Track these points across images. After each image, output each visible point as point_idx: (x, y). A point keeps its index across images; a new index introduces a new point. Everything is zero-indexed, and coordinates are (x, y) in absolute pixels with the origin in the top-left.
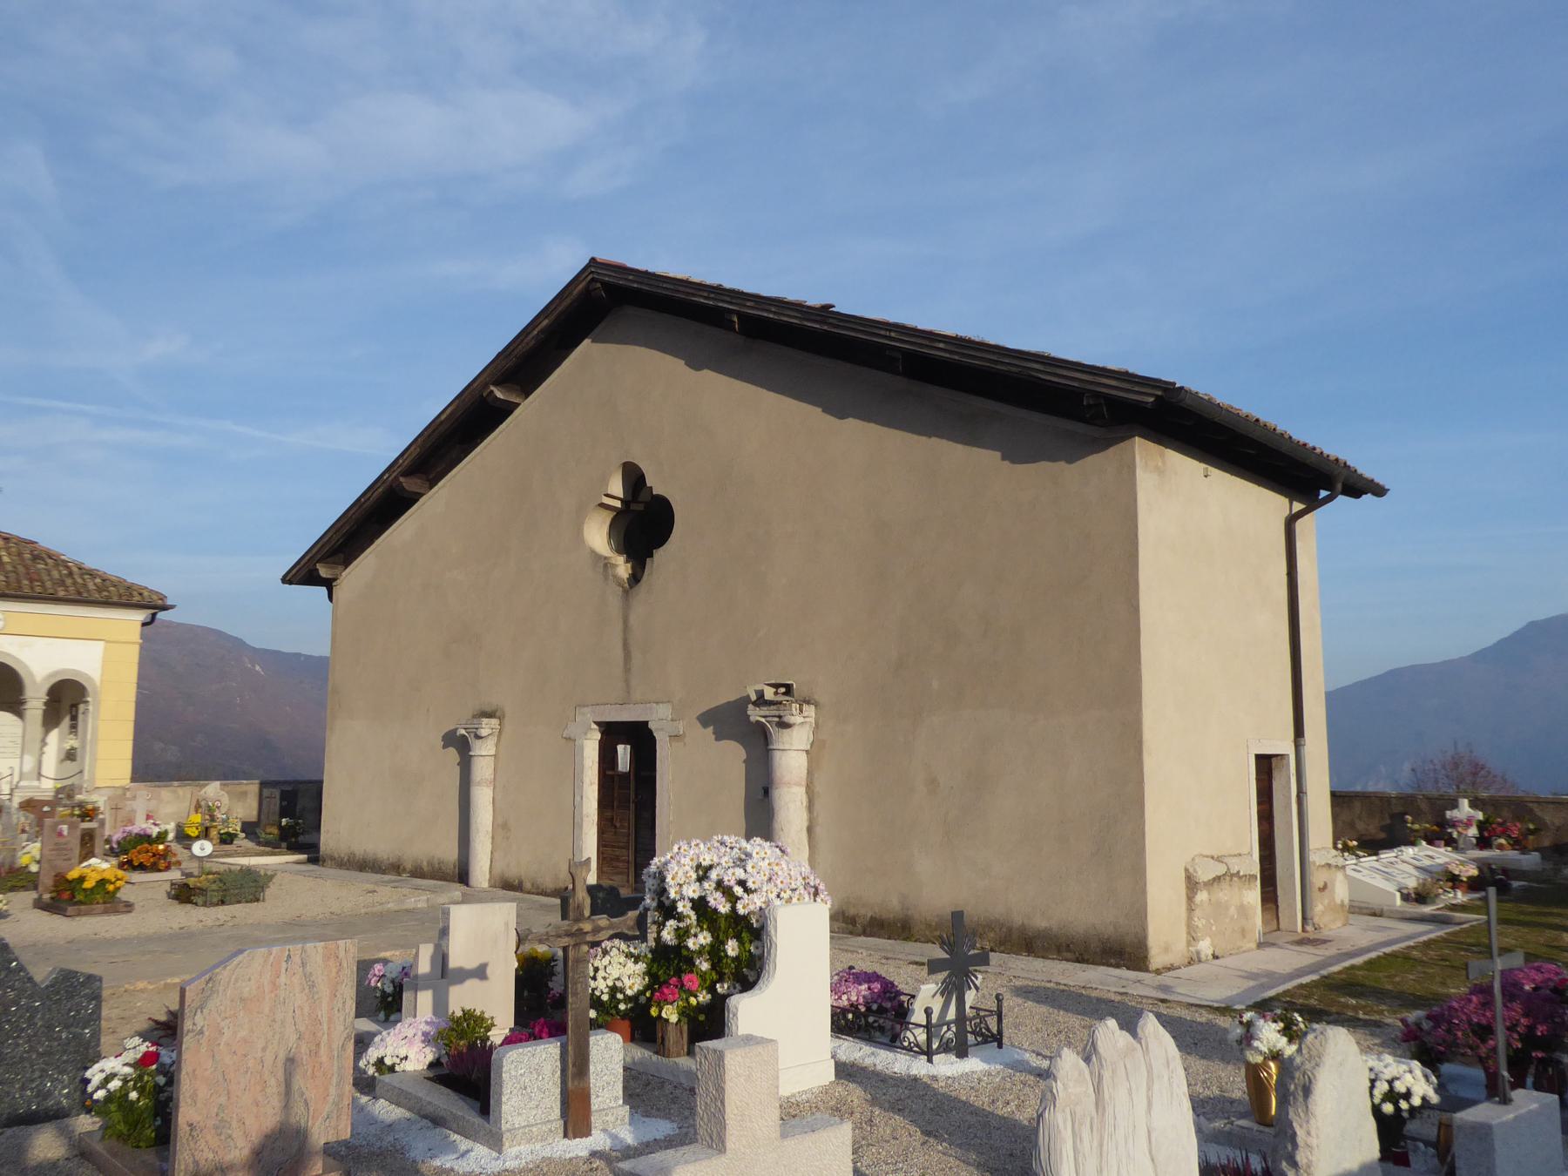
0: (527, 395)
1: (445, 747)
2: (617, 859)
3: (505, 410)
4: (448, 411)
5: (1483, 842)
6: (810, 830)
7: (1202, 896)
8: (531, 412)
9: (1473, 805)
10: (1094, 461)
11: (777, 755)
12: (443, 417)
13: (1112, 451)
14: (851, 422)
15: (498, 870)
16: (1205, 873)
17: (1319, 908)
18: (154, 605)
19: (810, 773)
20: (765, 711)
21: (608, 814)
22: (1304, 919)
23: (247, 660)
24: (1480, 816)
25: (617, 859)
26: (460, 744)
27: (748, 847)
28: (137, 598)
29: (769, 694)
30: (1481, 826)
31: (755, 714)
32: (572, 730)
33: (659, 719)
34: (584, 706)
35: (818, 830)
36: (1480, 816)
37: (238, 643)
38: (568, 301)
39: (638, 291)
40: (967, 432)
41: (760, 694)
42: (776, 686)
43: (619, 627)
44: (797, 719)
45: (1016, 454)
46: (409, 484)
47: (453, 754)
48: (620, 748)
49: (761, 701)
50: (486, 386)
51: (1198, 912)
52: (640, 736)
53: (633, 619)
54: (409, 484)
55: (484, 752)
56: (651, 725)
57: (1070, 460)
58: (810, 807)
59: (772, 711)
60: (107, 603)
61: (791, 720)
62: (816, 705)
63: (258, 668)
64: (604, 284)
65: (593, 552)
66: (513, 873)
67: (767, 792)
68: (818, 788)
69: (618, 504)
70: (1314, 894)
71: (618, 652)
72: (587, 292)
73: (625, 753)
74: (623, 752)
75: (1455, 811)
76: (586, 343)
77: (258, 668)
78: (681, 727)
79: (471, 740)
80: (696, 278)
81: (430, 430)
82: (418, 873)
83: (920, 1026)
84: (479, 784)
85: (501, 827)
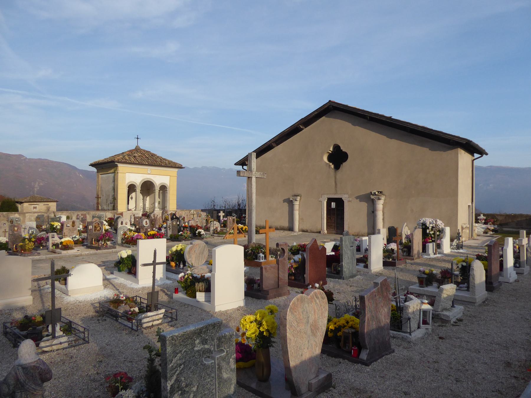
0: (305, 128)
1: (283, 202)
2: (332, 225)
3: (301, 130)
4: (287, 130)
5: (485, 223)
6: (383, 219)
7: (464, 230)
8: (306, 131)
9: (483, 216)
10: (450, 152)
11: (377, 205)
12: (286, 131)
13: (454, 151)
14: (393, 140)
15: (301, 228)
16: (464, 226)
17: (474, 234)
18: (180, 167)
19: (383, 208)
20: (375, 196)
21: (329, 216)
22: (472, 236)
23: (77, 173)
24: (485, 218)
25: (332, 225)
26: (290, 203)
27: (48, 235)
28: (177, 166)
29: (377, 193)
30: (485, 220)
31: (372, 197)
32: (321, 199)
33: (345, 198)
34: (324, 194)
35: (385, 219)
36: (485, 218)
37: (74, 168)
38: (322, 109)
39: (342, 109)
40: (421, 144)
41: (375, 193)
42: (378, 192)
43: (334, 178)
44: (382, 198)
45: (432, 149)
46: (274, 145)
47: (286, 204)
48: (332, 203)
49: (375, 194)
50: (298, 125)
51: (463, 233)
52: (340, 202)
53: (338, 177)
54: (274, 145)
55: (297, 204)
56: (343, 199)
57: (444, 151)
58: (383, 215)
59: (377, 196)
60: (172, 167)
61: (381, 198)
62: (385, 195)
63: (81, 175)
64: (333, 106)
65: (325, 162)
66: (305, 228)
67: (373, 212)
68: (385, 211)
69: (331, 152)
70: (473, 231)
71: (334, 183)
72: (328, 107)
73: (334, 204)
74: (333, 205)
75: (480, 217)
76: (324, 117)
77: (81, 175)
78: (351, 199)
79: (294, 201)
80: (358, 107)
81: (281, 134)
82: (277, 229)
83: (146, 299)
84: (296, 210)
85: (301, 219)
